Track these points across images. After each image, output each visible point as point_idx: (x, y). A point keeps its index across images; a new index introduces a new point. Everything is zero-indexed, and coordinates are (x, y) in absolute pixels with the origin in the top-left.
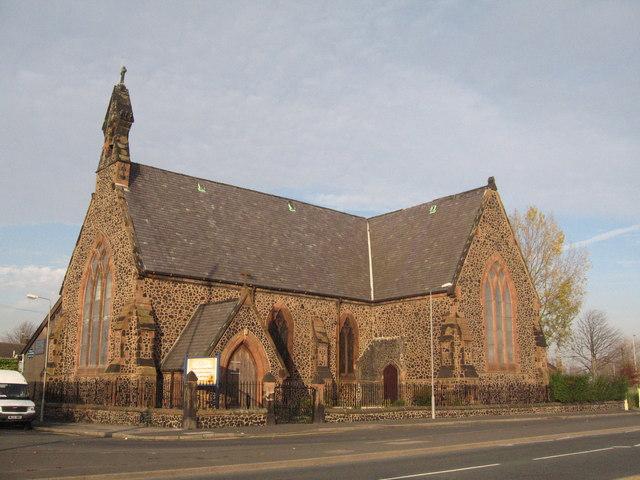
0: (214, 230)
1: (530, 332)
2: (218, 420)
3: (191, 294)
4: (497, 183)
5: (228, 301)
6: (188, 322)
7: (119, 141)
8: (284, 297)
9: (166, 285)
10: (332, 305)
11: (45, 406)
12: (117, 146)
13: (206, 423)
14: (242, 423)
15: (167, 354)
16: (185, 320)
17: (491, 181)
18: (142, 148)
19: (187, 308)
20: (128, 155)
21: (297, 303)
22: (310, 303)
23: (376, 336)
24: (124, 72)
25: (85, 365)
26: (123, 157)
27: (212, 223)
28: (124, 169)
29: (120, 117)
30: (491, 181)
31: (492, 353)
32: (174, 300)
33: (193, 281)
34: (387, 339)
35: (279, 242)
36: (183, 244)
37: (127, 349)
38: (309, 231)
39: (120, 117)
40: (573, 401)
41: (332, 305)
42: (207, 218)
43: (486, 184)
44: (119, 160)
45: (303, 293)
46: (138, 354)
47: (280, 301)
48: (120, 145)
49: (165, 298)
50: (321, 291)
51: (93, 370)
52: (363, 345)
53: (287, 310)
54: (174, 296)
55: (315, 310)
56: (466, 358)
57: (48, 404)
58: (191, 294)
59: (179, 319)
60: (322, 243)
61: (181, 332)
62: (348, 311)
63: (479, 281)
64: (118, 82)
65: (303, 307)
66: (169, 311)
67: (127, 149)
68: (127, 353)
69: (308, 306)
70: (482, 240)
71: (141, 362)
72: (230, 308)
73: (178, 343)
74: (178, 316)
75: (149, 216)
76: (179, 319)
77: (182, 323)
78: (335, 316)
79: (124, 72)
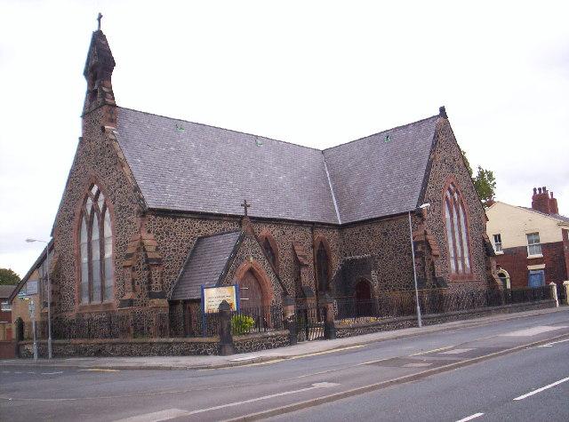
4: (448, 112)
10: (308, 230)
11: (53, 344)
17: (442, 110)
18: (126, 90)
19: (187, 241)
24: (100, 17)
25: (85, 301)
29: (100, 64)
30: (442, 110)
33: (190, 216)
34: (358, 257)
39: (100, 64)
43: (438, 113)
45: (284, 220)
48: (105, 89)
49: (167, 233)
51: (97, 306)
52: (336, 264)
56: (303, 280)
57: (424, 316)
61: (183, 264)
64: (96, 29)
67: (112, 93)
68: (138, 287)
76: (181, 252)
78: (308, 242)
79: (100, 17)
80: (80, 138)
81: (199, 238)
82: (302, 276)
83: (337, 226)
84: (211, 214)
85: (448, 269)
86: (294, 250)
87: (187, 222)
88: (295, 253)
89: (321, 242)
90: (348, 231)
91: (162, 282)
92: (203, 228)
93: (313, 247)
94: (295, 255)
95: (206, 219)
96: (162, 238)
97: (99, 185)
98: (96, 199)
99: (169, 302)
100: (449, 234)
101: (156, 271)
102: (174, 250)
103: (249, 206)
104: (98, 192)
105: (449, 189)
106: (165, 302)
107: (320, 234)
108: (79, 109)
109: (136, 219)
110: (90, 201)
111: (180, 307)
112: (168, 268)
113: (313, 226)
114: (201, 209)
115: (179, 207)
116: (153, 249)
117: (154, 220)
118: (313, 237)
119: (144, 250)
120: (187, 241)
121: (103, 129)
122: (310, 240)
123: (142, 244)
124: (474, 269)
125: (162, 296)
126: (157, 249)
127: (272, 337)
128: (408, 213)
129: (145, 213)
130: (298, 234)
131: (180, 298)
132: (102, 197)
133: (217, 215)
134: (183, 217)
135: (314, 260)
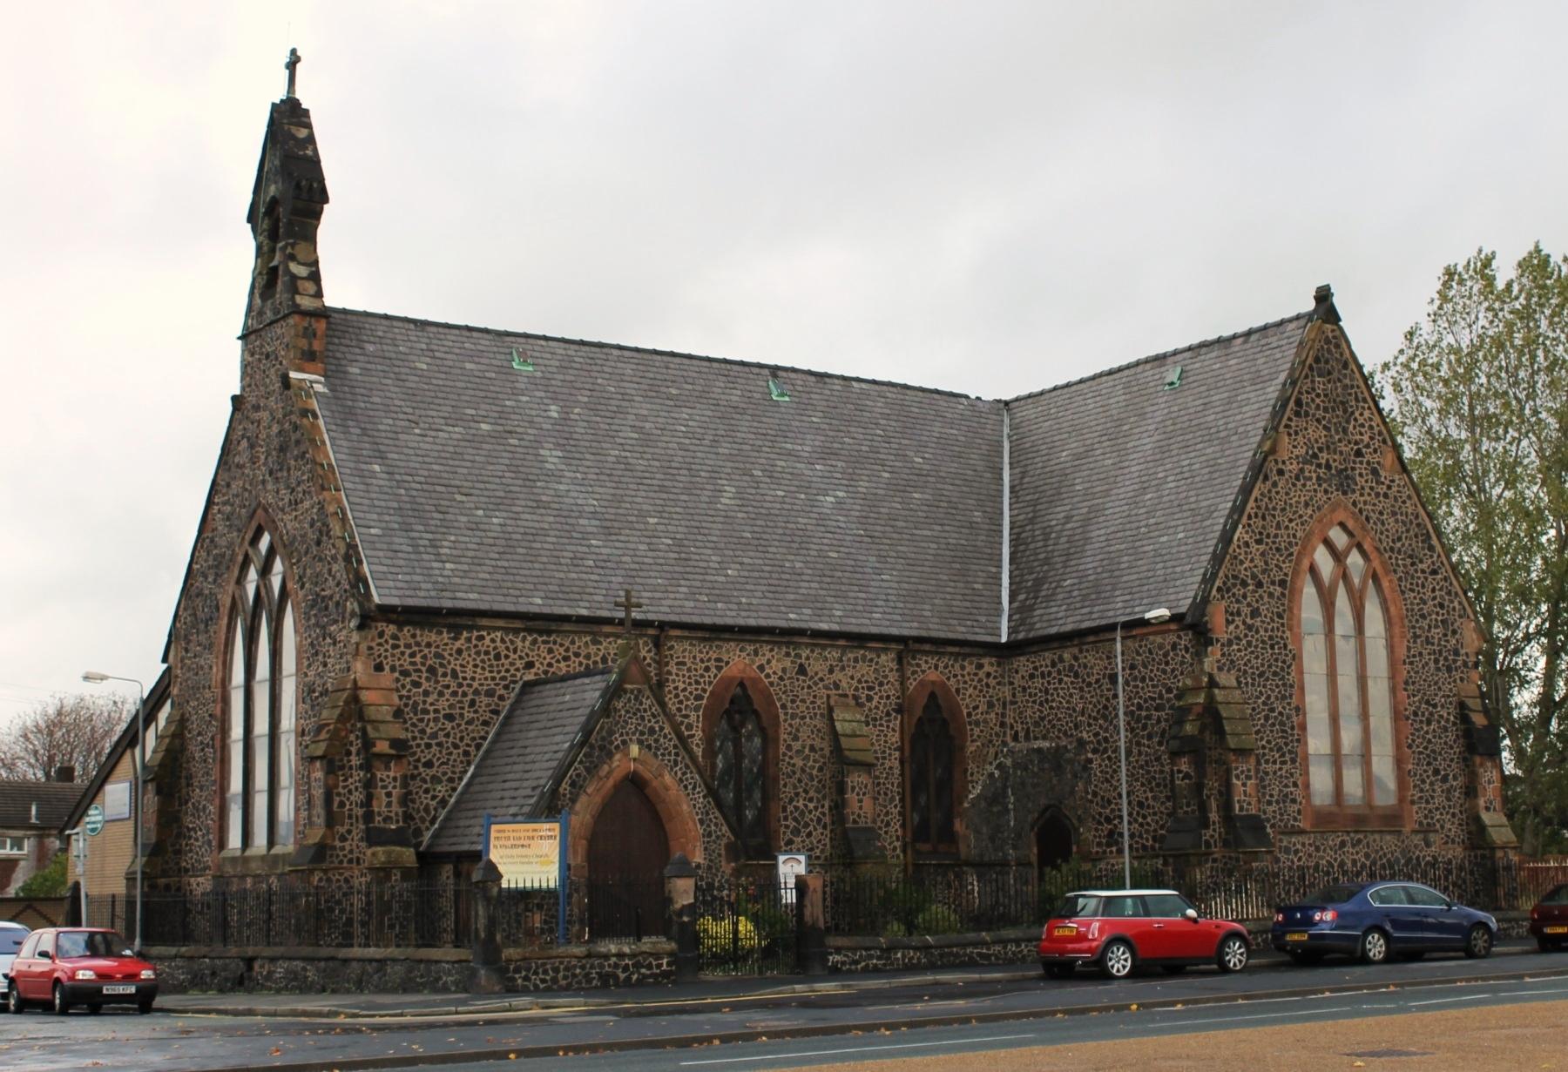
0: (556, 476)
1: (1448, 713)
2: (556, 970)
3: (497, 657)
4: (1337, 301)
5: (588, 673)
6: (508, 703)
7: (292, 258)
8: (750, 648)
9: (433, 637)
10: (887, 660)
12: (288, 271)
13: (526, 978)
14: (616, 977)
15: (443, 814)
16: (485, 723)
17: (1324, 296)
19: (490, 693)
20: (319, 294)
21: (787, 663)
22: (818, 662)
23: (1015, 738)
24: (293, 63)
26: (305, 302)
27: (552, 457)
28: (309, 334)
30: (1324, 296)
31: (1320, 780)
32: (454, 674)
33: (500, 623)
35: (739, 495)
36: (475, 527)
37: (342, 805)
38: (827, 454)
40: (836, 901)
41: (887, 660)
42: (538, 443)
43: (1310, 305)
44: (297, 310)
45: (801, 632)
46: (369, 817)
47: (738, 660)
48: (295, 268)
49: (432, 670)
50: (856, 625)
53: (756, 681)
54: (455, 664)
55: (837, 675)
58: (497, 657)
59: (469, 722)
60: (863, 486)
62: (933, 676)
63: (1282, 583)
64: (279, 94)
65: (802, 670)
66: (443, 704)
67: (315, 277)
69: (817, 666)
70: (1293, 467)
71: (374, 837)
72: (591, 693)
73: (469, 784)
74: (468, 715)
75: (382, 457)
76: (469, 722)
77: (476, 730)
79: (293, 63)
80: (235, 399)
81: (528, 686)
82: (851, 796)
83: (994, 649)
84: (566, 619)
85: (1298, 793)
86: (832, 720)
87: (493, 639)
88: (833, 727)
89: (932, 696)
90: (1023, 664)
91: (405, 800)
92: (542, 654)
93: (900, 710)
94: (835, 735)
95: (549, 633)
96: (416, 684)
97: (274, 530)
98: (265, 571)
99: (421, 856)
100: (288, 721)
101: (388, 776)
102: (450, 717)
103: (628, 596)
104: (272, 551)
105: (1328, 543)
106: (408, 855)
107: (928, 670)
108: (237, 325)
109: (348, 633)
110: (253, 575)
111: (447, 871)
112: (429, 764)
113: (907, 647)
114: (536, 603)
115: (470, 600)
116: (385, 713)
117: (395, 637)
118: (903, 680)
119: (361, 718)
120: (490, 693)
121: (286, 383)
122: (892, 689)
123: (355, 699)
124: (1413, 793)
125: (399, 838)
126: (398, 713)
127: (621, 955)
128: (1112, 628)
129: (370, 617)
130: (858, 670)
131: (445, 847)
132: (278, 566)
133: (581, 620)
134: (480, 628)
135: (901, 749)
